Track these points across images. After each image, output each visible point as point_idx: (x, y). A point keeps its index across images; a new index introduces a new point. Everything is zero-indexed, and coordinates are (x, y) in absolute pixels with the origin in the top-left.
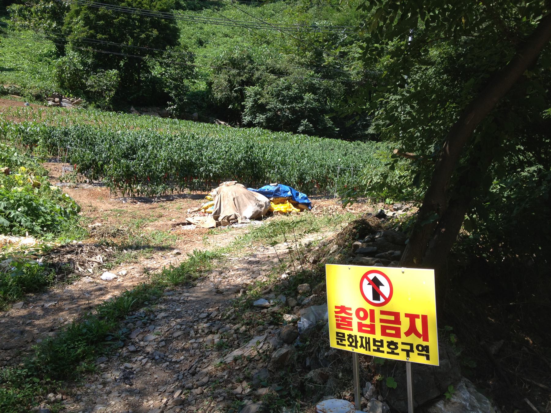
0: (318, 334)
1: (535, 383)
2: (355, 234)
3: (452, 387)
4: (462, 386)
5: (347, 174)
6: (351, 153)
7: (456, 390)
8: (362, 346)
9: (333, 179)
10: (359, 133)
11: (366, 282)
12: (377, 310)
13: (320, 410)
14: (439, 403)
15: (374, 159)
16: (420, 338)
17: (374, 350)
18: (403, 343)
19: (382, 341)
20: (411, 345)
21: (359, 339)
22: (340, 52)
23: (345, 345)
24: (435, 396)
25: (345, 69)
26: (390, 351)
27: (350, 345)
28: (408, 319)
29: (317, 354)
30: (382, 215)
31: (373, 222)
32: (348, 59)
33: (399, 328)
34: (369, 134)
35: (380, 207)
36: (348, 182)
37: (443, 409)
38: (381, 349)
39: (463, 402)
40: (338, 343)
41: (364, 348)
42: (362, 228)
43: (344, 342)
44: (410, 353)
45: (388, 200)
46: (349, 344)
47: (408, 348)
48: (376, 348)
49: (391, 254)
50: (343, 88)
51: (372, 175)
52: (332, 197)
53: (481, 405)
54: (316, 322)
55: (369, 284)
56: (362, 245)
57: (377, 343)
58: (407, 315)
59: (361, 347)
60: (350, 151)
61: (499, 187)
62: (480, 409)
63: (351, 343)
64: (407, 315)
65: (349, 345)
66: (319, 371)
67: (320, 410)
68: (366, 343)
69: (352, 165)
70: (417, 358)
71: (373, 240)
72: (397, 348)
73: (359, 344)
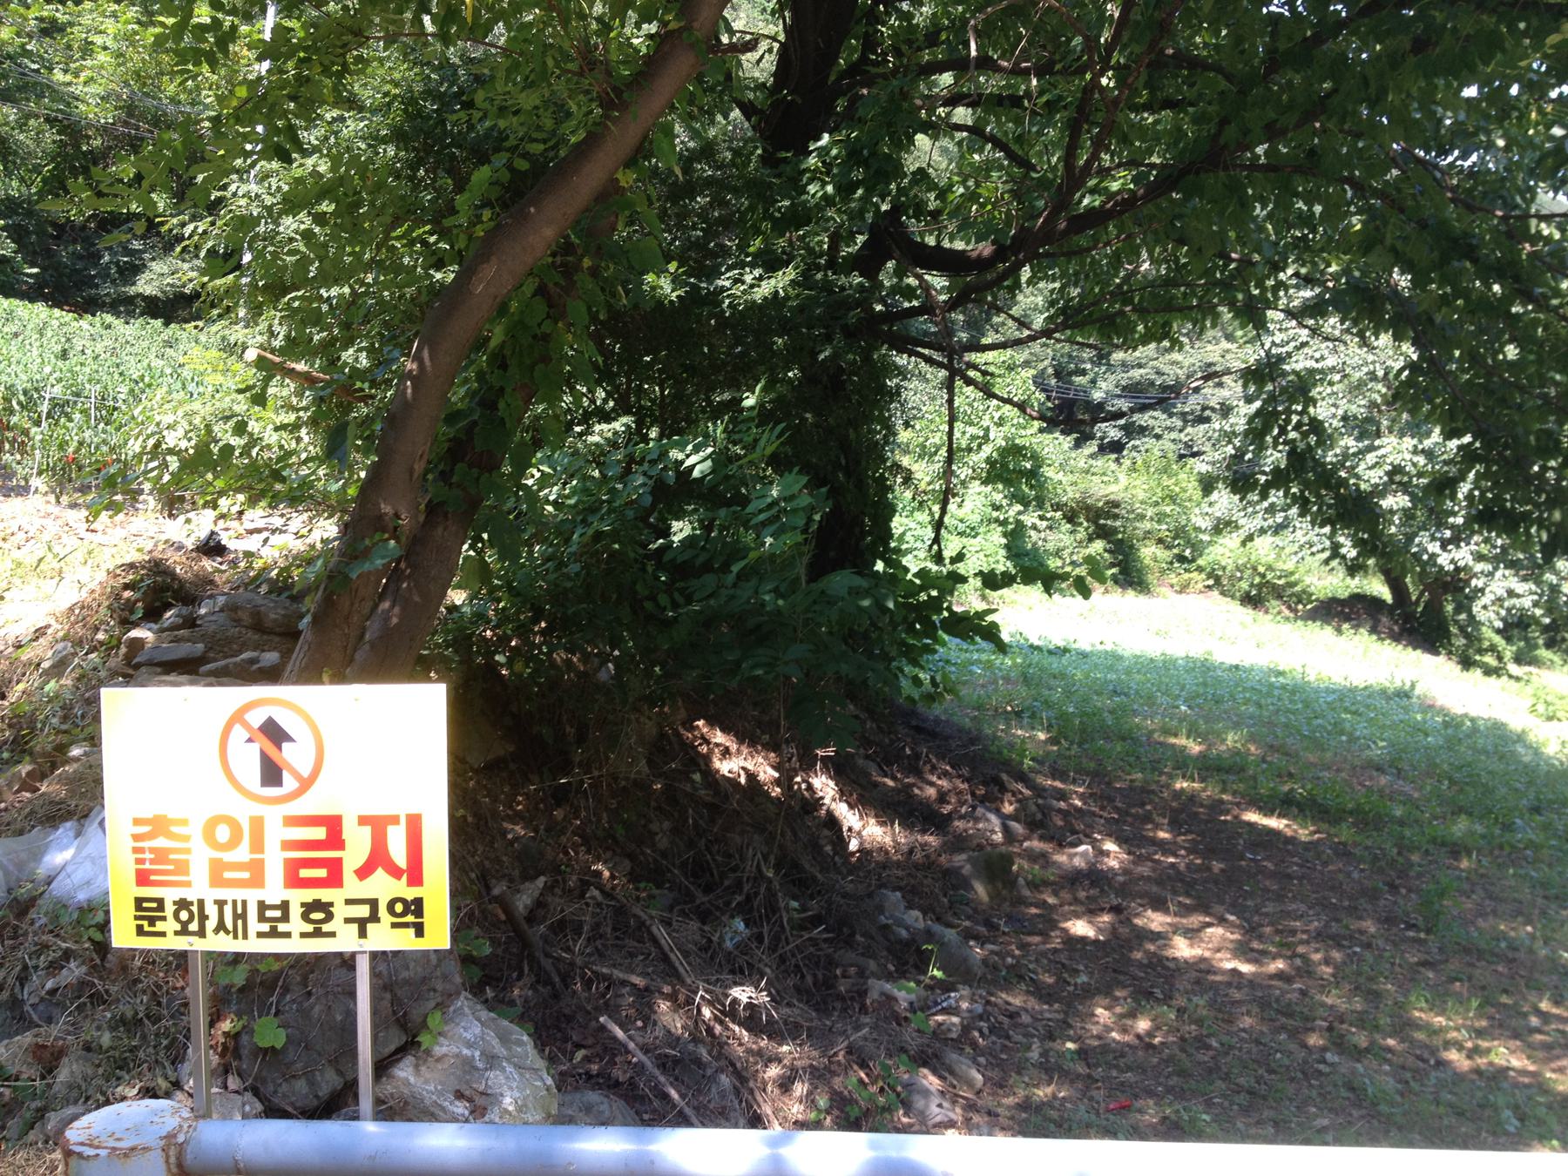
0: (16, 928)
1: (621, 975)
2: (130, 606)
3: (438, 1015)
4: (461, 1008)
5: (77, 416)
6: (83, 352)
7: (446, 1023)
8: (221, 926)
9: (26, 432)
10: (107, 290)
11: (239, 733)
12: (273, 817)
13: (82, 1144)
14: (401, 1065)
15: (194, 378)
16: (399, 877)
17: (260, 935)
18: (349, 902)
19: (284, 906)
20: (373, 903)
21: (211, 911)
22: (41, 19)
23: (163, 934)
24: (392, 1048)
25: (58, 76)
26: (310, 928)
27: (184, 931)
28: (368, 830)
29: (17, 990)
30: (212, 547)
31: (179, 565)
32: (69, 47)
33: (339, 861)
34: (139, 295)
35: (202, 523)
36: (81, 443)
37: (412, 1080)
38: (282, 927)
39: (466, 1052)
40: (140, 931)
41: (227, 932)
42: (156, 591)
43: (160, 926)
44: (369, 926)
45: (224, 503)
46: (178, 927)
47: (364, 911)
48: (265, 927)
49: (253, 661)
50: (50, 136)
51: (173, 420)
52: (23, 490)
53: (509, 1049)
54: (9, 891)
55: (250, 740)
56: (159, 639)
57: (269, 914)
58: (363, 820)
59: (217, 931)
60: (78, 344)
61: (538, 475)
62: (508, 1060)
63: (185, 925)
64: (363, 820)
65: (177, 933)
66: (27, 1039)
67: (82, 1144)
68: (236, 916)
69: (93, 390)
70: (387, 937)
71: (190, 622)
72: (329, 917)
73: (211, 924)
